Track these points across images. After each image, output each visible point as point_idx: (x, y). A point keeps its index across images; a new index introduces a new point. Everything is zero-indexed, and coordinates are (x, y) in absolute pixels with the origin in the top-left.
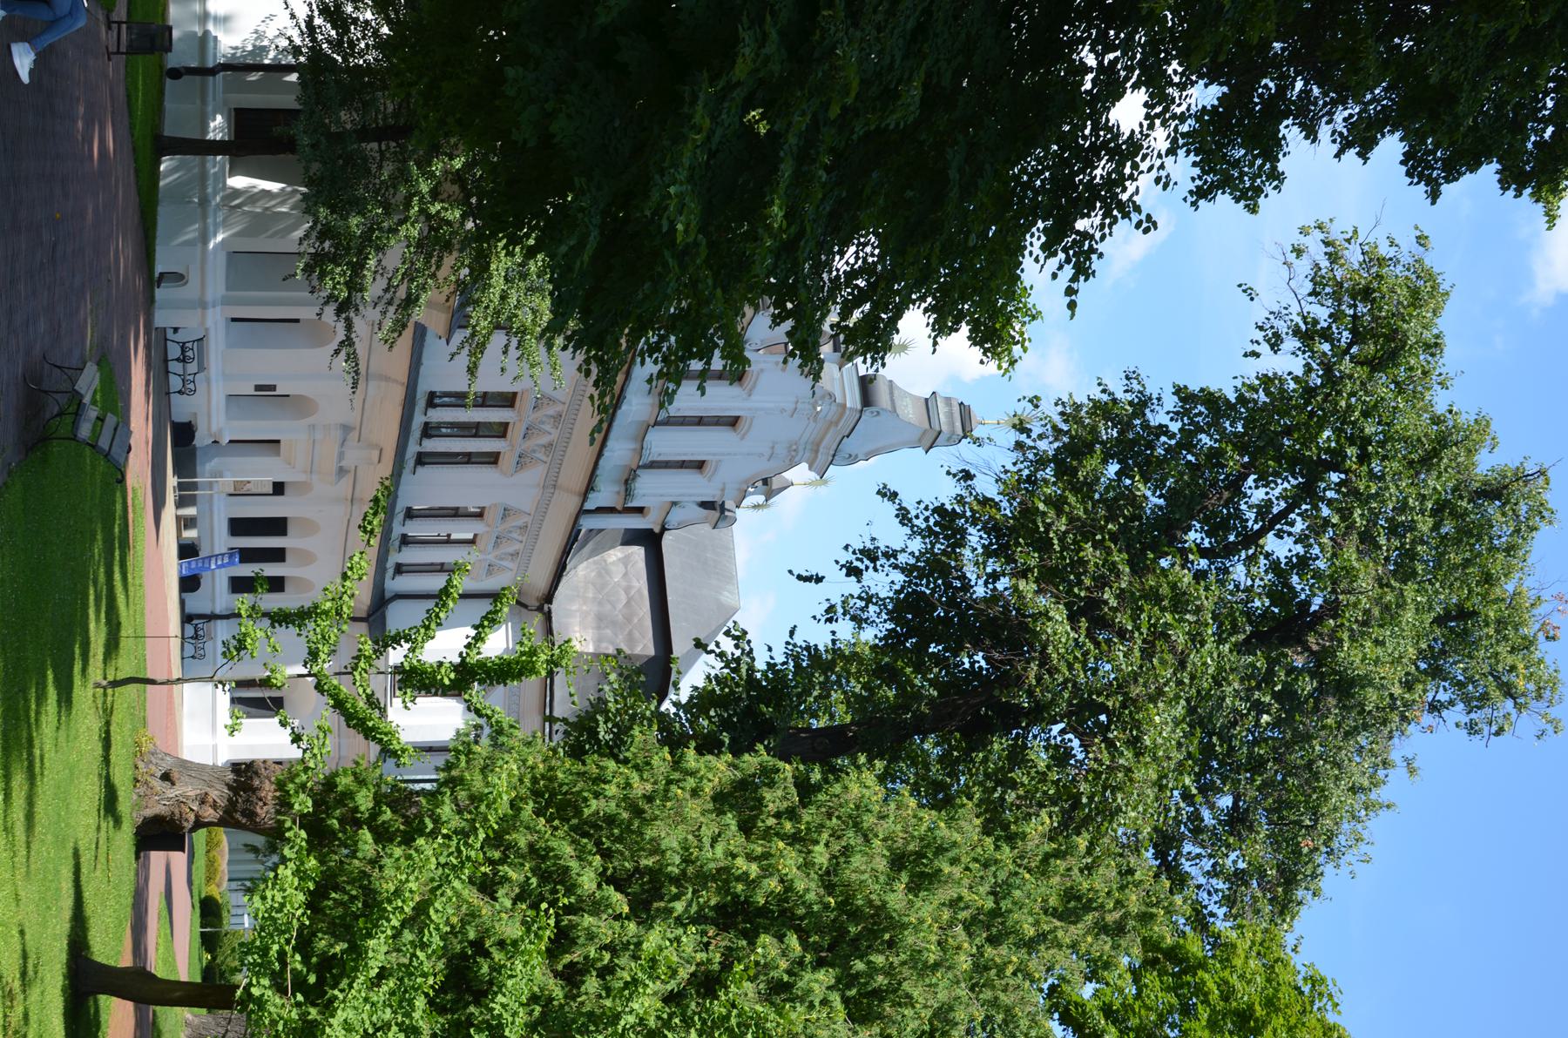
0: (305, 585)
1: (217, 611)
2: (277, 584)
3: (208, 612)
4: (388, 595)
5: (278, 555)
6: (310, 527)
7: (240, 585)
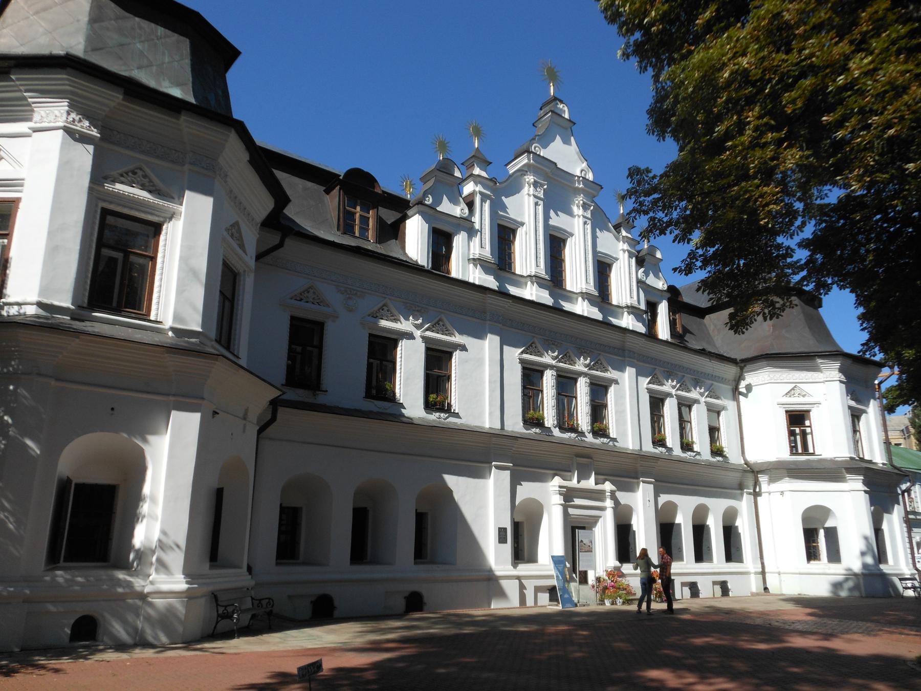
3: (767, 570)
7: (732, 552)
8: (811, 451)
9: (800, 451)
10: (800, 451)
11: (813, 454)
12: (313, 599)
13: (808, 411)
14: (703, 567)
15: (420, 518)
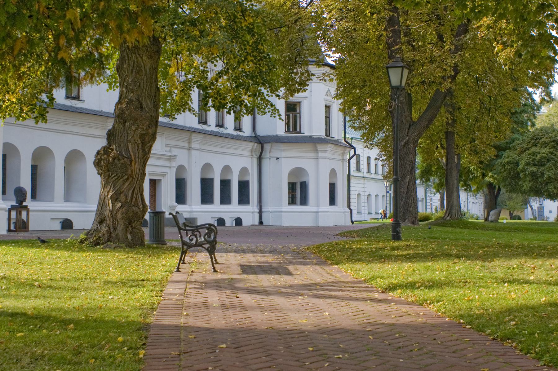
0: (244, 171)
1: (258, 211)
2: (244, 186)
3: (263, 210)
4: (254, 135)
5: (225, 184)
6: (207, 167)
7: (244, 199)
8: (298, 130)
9: (291, 130)
10: (291, 130)
11: (300, 132)
12: (61, 220)
13: (300, 103)
14: (225, 208)
15: (34, 169)
